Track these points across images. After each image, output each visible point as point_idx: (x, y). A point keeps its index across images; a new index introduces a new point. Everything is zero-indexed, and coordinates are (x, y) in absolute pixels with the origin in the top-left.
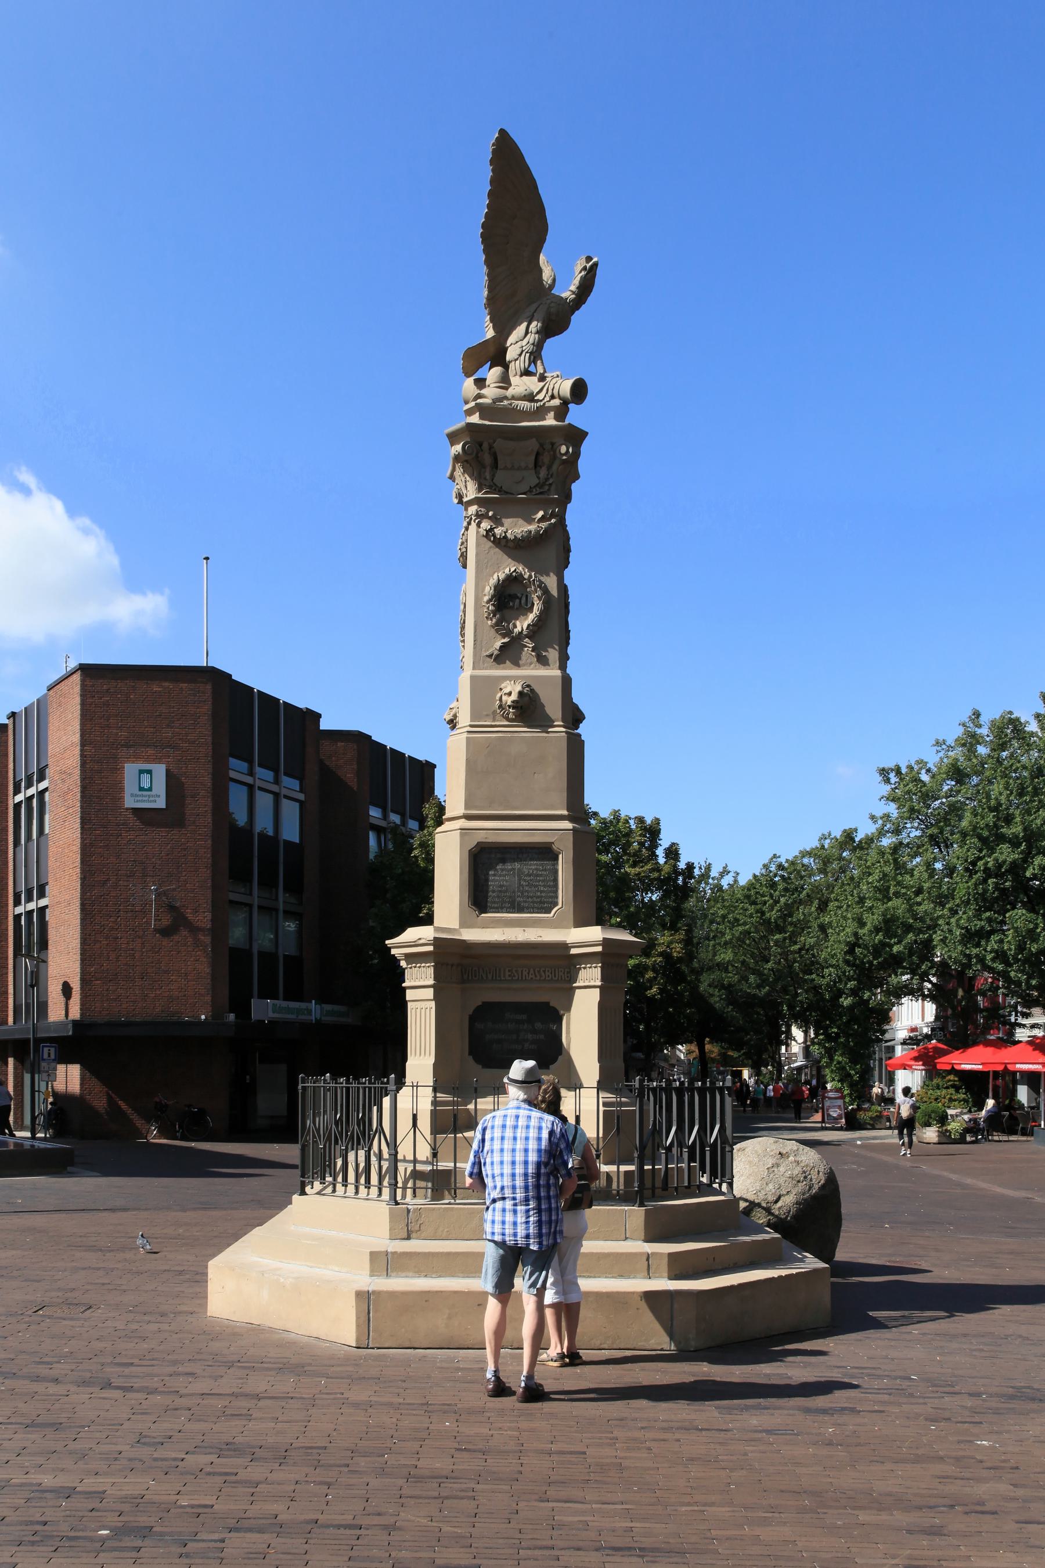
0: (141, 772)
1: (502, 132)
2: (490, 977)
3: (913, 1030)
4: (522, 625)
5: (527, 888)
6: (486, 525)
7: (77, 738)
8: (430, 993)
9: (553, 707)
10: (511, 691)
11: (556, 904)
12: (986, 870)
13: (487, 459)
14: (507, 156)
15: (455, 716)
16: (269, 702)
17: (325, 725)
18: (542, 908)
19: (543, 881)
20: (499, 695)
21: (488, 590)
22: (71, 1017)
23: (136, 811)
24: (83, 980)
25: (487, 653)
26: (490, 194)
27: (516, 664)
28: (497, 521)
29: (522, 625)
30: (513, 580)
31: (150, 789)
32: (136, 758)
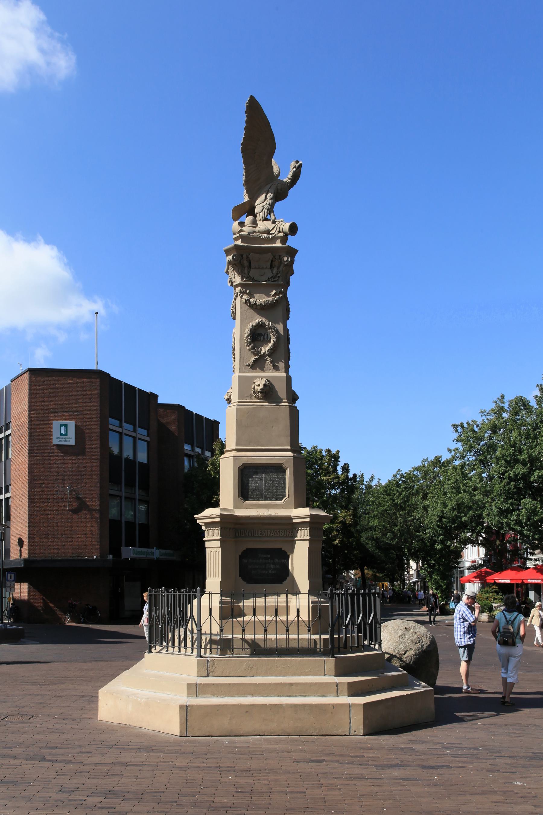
0: (62, 425)
1: (252, 97)
2: (250, 535)
3: (474, 562)
4: (265, 349)
5: (269, 488)
6: (245, 297)
7: (26, 407)
8: (218, 543)
9: (282, 392)
10: (260, 384)
11: (285, 496)
12: (510, 478)
13: (246, 263)
14: (254, 109)
15: (230, 397)
16: (130, 389)
17: (160, 401)
18: (278, 498)
19: (278, 484)
20: (253, 386)
21: (247, 331)
22: (23, 557)
23: (58, 446)
24: (30, 537)
25: (247, 364)
26: (246, 128)
27: (262, 369)
28: (251, 295)
29: (265, 349)
30: (260, 326)
31: (66, 435)
32: (59, 418)
